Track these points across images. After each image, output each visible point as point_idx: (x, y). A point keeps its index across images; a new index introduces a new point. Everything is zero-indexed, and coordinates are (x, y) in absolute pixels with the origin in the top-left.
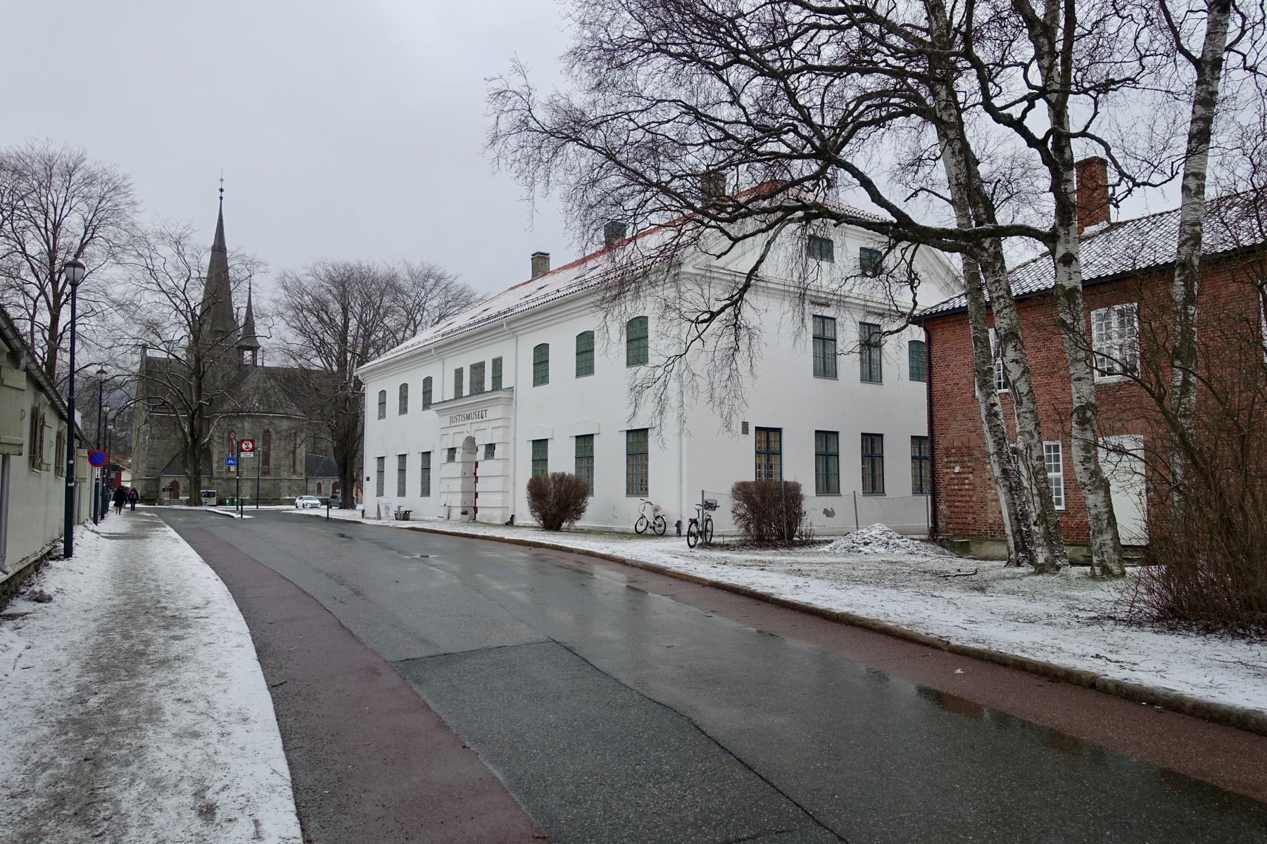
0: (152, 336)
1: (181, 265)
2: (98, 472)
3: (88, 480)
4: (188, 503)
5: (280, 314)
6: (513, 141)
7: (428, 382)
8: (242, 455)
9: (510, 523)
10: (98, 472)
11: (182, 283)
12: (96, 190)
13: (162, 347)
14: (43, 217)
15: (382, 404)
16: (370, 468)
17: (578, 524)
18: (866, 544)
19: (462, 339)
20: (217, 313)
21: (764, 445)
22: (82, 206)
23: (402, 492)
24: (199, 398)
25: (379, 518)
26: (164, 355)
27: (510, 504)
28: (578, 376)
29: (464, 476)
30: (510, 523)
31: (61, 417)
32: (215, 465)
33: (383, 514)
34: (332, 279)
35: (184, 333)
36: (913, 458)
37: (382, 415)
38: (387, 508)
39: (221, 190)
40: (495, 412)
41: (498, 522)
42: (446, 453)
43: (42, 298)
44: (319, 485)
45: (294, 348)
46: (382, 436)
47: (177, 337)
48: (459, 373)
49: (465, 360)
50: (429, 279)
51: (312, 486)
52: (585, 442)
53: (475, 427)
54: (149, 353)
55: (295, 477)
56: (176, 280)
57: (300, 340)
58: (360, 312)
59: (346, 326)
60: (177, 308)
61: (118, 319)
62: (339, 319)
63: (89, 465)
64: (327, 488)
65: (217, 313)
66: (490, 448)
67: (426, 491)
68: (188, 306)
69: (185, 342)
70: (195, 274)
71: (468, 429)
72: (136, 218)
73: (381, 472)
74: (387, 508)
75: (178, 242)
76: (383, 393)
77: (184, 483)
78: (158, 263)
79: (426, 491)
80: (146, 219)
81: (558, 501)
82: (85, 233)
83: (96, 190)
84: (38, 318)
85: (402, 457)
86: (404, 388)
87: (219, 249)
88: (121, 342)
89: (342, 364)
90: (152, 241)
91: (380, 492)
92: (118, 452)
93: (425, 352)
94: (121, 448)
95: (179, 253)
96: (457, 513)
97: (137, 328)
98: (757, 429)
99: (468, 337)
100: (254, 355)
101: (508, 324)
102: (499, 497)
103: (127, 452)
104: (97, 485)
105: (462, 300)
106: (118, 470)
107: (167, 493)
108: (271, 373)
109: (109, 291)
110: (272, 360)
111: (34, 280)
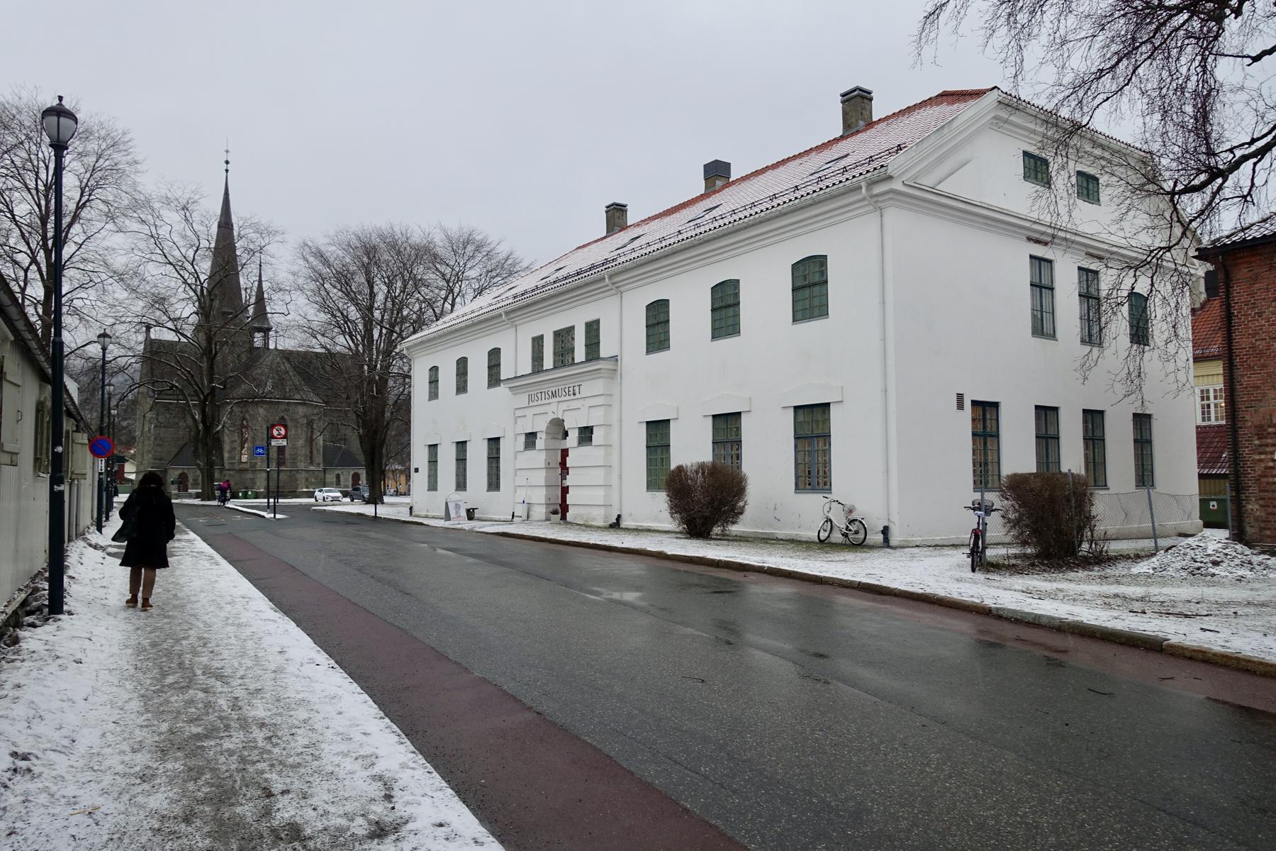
0: (158, 313)
1: (189, 233)
2: (101, 464)
3: (89, 476)
4: (197, 496)
5: (301, 289)
7: (495, 354)
8: (274, 443)
9: (616, 525)
10: (101, 464)
11: (190, 253)
14: (33, 176)
15: (434, 382)
16: (419, 457)
17: (734, 529)
18: (1216, 563)
19: (544, 300)
20: (224, 292)
21: (980, 426)
23: (461, 485)
24: (211, 381)
25: (447, 517)
27: (615, 500)
28: (714, 337)
29: (548, 467)
30: (616, 525)
31: (43, 377)
32: (226, 455)
33: (453, 514)
36: (1136, 441)
37: (434, 395)
38: (457, 507)
39: (227, 162)
40: (591, 387)
41: (601, 524)
42: (523, 438)
43: (34, 267)
44: (338, 477)
45: (315, 325)
46: (432, 421)
48: (538, 342)
49: (547, 326)
50: (467, 245)
51: (330, 477)
52: (727, 427)
53: (564, 406)
54: (155, 334)
55: (312, 468)
56: (183, 251)
57: (324, 317)
58: (390, 287)
59: (372, 295)
60: (185, 282)
61: (121, 294)
63: (89, 456)
64: (347, 480)
65: (224, 292)
66: (586, 434)
67: (494, 483)
70: (204, 244)
71: (554, 409)
73: (433, 462)
74: (457, 507)
75: (185, 208)
76: (434, 370)
77: (194, 474)
78: (163, 231)
79: (494, 483)
80: (149, 182)
81: (707, 499)
82: (82, 195)
84: (29, 291)
85: (462, 445)
86: (462, 364)
87: (225, 224)
90: (156, 205)
91: (433, 486)
92: (121, 443)
93: (493, 318)
94: (123, 438)
95: (186, 220)
96: (540, 512)
97: (141, 304)
98: (974, 403)
99: (552, 297)
100: (266, 338)
101: (611, 277)
102: (600, 493)
103: (130, 443)
104: (100, 481)
105: (503, 270)
106: (122, 460)
107: (175, 486)
108: (287, 355)
109: (110, 261)
110: (284, 341)
111: (25, 249)
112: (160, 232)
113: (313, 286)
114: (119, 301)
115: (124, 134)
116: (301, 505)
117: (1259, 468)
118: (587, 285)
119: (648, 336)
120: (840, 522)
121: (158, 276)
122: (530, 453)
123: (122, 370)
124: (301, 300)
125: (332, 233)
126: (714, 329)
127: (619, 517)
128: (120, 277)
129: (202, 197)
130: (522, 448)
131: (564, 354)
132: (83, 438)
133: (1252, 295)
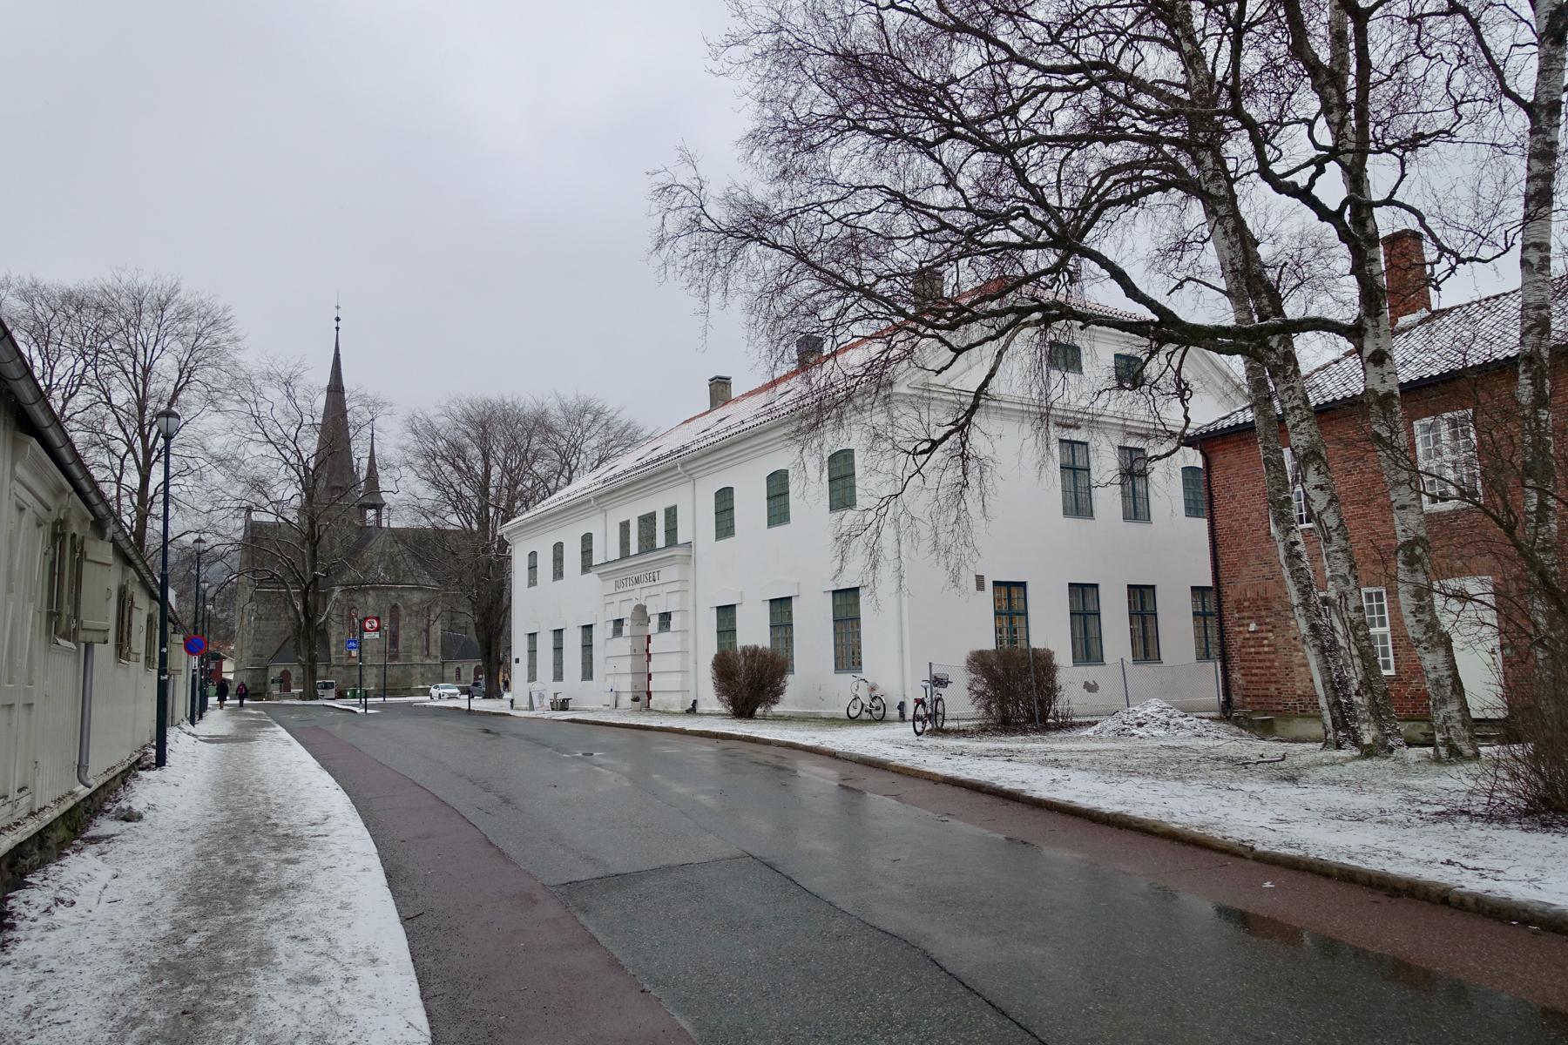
0: (258, 496)
1: (291, 409)
4: (301, 697)
5: (409, 464)
7: (587, 539)
9: (692, 711)
11: (293, 431)
12: (192, 325)
13: (269, 509)
14: (131, 360)
15: (533, 568)
16: (519, 647)
17: (776, 709)
18: (1140, 725)
19: (628, 486)
20: (334, 465)
21: (1005, 604)
22: (177, 346)
23: (558, 676)
24: (314, 568)
25: (532, 708)
26: (272, 519)
29: (634, 654)
30: (692, 711)
31: (152, 596)
32: (333, 649)
33: (536, 704)
34: (470, 420)
35: (296, 491)
37: (533, 581)
39: (338, 319)
40: (669, 573)
41: (678, 709)
42: (611, 626)
43: (130, 456)
44: (458, 671)
45: (426, 504)
46: (533, 608)
47: (287, 496)
48: (625, 527)
49: (632, 512)
50: (585, 415)
51: (450, 671)
52: (781, 607)
53: (646, 592)
54: (255, 517)
58: (506, 459)
59: (487, 475)
60: (287, 462)
62: (479, 468)
63: (184, 654)
65: (334, 465)
66: (665, 618)
67: (588, 674)
68: (300, 458)
69: (296, 502)
70: (307, 420)
71: (637, 595)
72: (239, 357)
73: (532, 652)
74: (541, 696)
75: (287, 383)
76: (533, 555)
77: (296, 672)
79: (588, 674)
80: (249, 359)
81: (751, 681)
83: (192, 325)
84: (125, 480)
85: (558, 633)
86: (558, 548)
87: (336, 389)
89: (484, 521)
90: (257, 383)
91: (532, 677)
92: (218, 637)
94: (222, 633)
95: (289, 396)
96: (626, 700)
99: (634, 483)
100: (378, 515)
102: (677, 678)
103: (229, 637)
105: (627, 438)
106: (219, 659)
108: (399, 535)
109: (208, 444)
110: (399, 520)
111: (121, 435)
113: (422, 462)
114: (222, 480)
115: (225, 311)
116: (410, 703)
117: (1240, 639)
118: (663, 472)
119: (717, 523)
120: (865, 698)
121: (259, 457)
122: (617, 640)
123: (220, 558)
124: (409, 476)
125: (444, 403)
126: (769, 517)
127: (695, 702)
128: (221, 461)
129: (306, 369)
130: (610, 634)
131: (648, 544)
132: (179, 638)
133: (1227, 479)
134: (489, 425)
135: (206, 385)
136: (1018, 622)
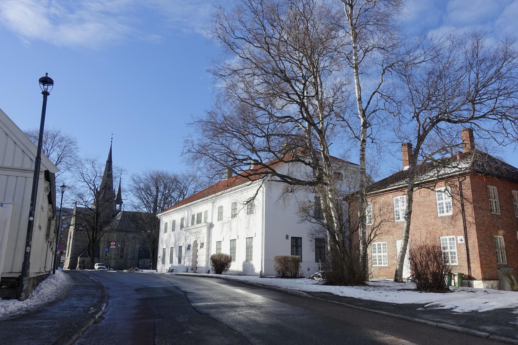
0: (80, 199)
1: (93, 171)
5: (131, 191)
6: (187, 156)
11: (93, 178)
12: (64, 144)
13: (83, 204)
16: (160, 254)
20: (107, 193)
22: (58, 149)
26: (84, 207)
32: (101, 253)
34: (152, 178)
35: (93, 198)
45: (136, 204)
47: (90, 200)
54: (77, 206)
56: (91, 177)
59: (157, 196)
60: (91, 188)
62: (155, 193)
65: (107, 193)
68: (95, 187)
69: (93, 202)
70: (98, 175)
72: (78, 154)
78: (85, 170)
80: (81, 154)
83: (64, 144)
87: (110, 162)
88: (67, 202)
89: (155, 210)
95: (93, 167)
98: (292, 237)
100: (121, 206)
108: (126, 214)
112: (84, 170)
134: (158, 180)
135: (66, 163)
136: (299, 248)
